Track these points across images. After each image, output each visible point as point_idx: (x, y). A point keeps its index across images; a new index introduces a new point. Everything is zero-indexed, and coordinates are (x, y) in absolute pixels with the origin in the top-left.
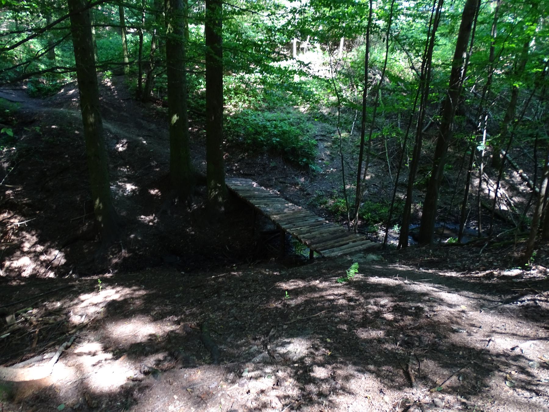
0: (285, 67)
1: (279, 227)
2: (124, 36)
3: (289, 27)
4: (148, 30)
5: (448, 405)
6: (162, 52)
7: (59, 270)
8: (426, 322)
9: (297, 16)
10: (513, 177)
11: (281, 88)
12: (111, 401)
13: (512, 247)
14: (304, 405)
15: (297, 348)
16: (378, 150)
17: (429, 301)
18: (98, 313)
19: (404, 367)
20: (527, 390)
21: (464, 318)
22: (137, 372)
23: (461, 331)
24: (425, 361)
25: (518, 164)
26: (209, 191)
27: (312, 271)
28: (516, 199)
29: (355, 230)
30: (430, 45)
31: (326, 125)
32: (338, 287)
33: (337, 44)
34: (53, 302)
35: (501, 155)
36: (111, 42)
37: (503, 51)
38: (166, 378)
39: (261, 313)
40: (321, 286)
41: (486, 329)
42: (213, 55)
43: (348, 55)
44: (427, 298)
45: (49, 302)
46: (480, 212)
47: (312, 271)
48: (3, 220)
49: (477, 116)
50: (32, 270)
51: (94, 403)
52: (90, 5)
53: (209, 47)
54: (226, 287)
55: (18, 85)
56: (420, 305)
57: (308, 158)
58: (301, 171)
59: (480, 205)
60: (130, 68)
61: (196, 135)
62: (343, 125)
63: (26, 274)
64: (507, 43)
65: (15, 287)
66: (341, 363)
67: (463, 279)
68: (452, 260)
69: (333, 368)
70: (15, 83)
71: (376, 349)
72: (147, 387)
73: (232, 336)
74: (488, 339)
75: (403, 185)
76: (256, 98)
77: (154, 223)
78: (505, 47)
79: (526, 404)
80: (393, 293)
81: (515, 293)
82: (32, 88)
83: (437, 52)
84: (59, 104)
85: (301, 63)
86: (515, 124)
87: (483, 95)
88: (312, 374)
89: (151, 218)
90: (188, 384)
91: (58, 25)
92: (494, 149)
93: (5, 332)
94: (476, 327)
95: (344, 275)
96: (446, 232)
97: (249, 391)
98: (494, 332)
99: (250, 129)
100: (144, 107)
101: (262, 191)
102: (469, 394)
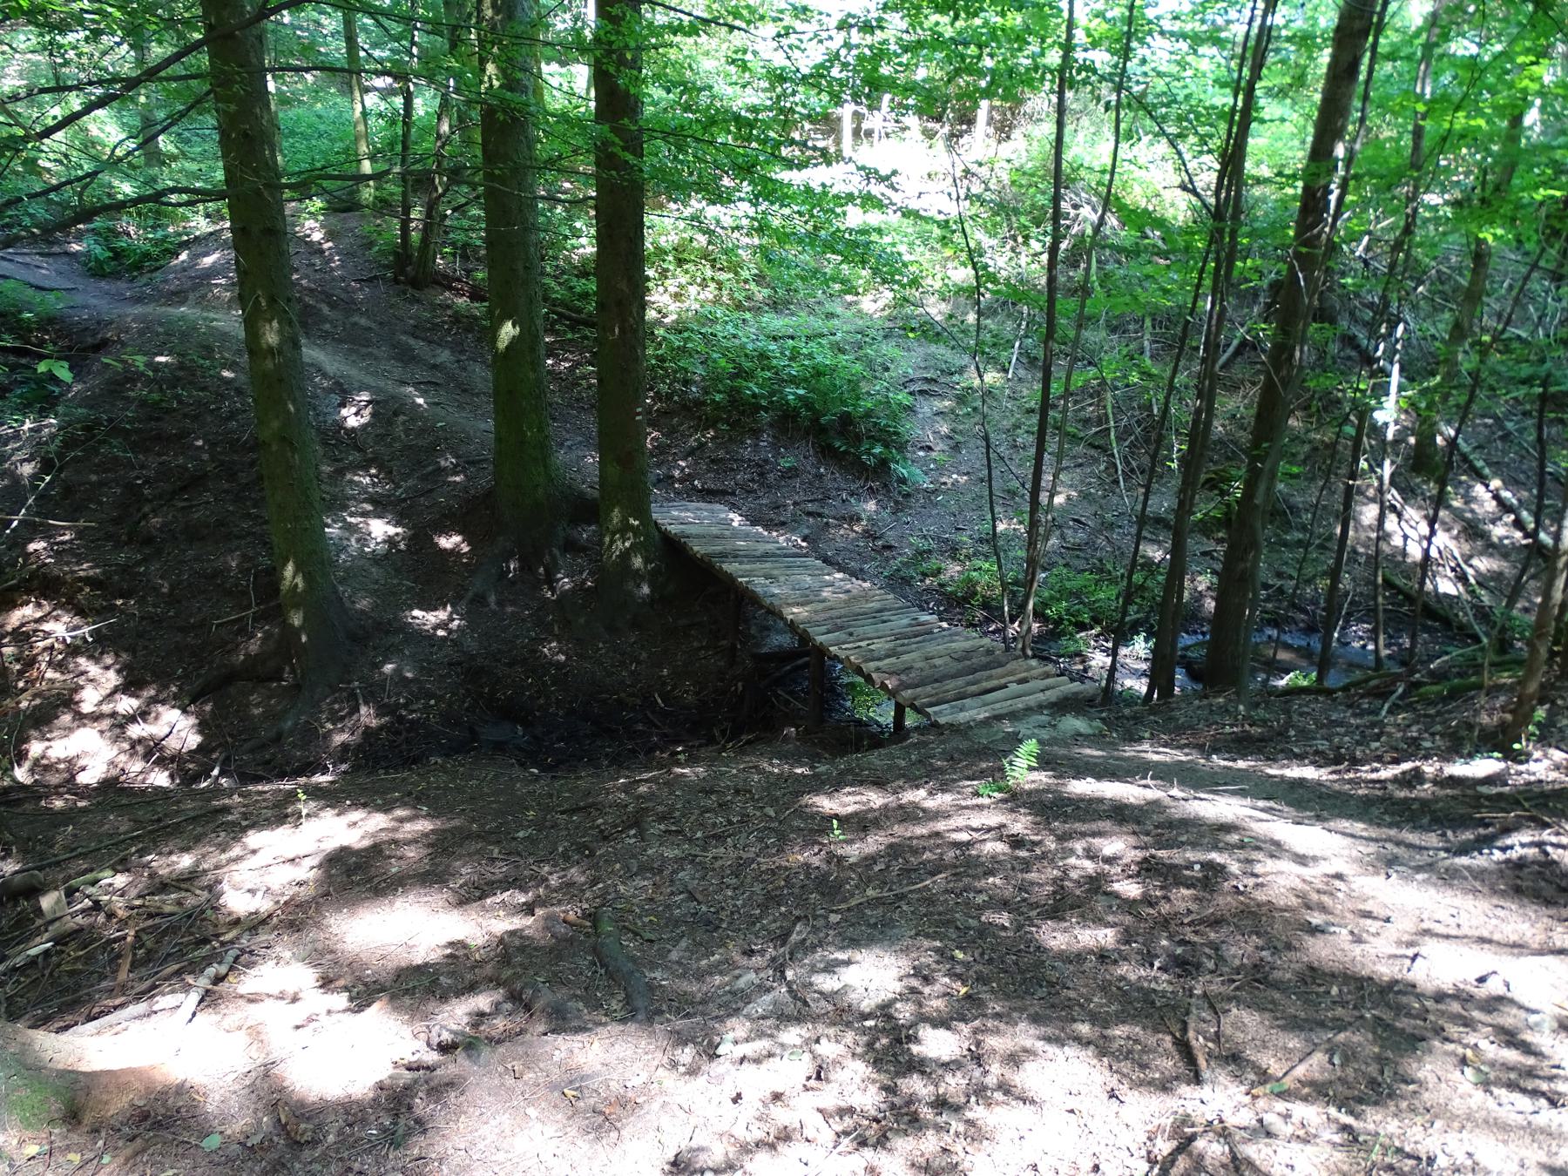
0: (824, 185)
1: (804, 638)
2: (353, 101)
3: (835, 72)
4: (431, 80)
5: (1301, 1133)
6: (467, 142)
7: (186, 767)
8: (1234, 904)
9: (856, 37)
10: (1475, 499)
11: (812, 244)
12: (350, 1125)
13: (1473, 698)
14: (897, 1132)
15: (873, 975)
16: (1086, 422)
17: (1242, 846)
18: (300, 884)
19: (1176, 1028)
20: (1524, 1091)
21: (1340, 895)
22: (420, 1044)
23: (1332, 929)
24: (1235, 1011)
25: (1489, 464)
26: (607, 539)
27: (903, 763)
28: (1483, 564)
29: (1023, 649)
30: (1242, 120)
31: (940, 350)
32: (980, 807)
33: (968, 120)
34: (171, 853)
35: (1439, 439)
36: (320, 117)
37: (1446, 140)
38: (502, 1062)
39: (763, 881)
40: (930, 804)
41: (1404, 925)
42: (617, 150)
43: (1004, 153)
44: (1234, 838)
45: (160, 854)
46: (1380, 599)
47: (903, 763)
48: (23, 625)
49: (1372, 327)
50: (105, 768)
51: (305, 1131)
52: (264, 13)
53: (606, 128)
54: (660, 809)
55: (57, 242)
56: (1215, 856)
57: (886, 446)
58: (867, 480)
59: (1380, 580)
60: (377, 189)
61: (569, 382)
62: (985, 352)
63: (88, 778)
64: (1461, 114)
65: (61, 812)
66: (998, 1016)
67: (1337, 786)
68: (1304, 734)
69: (975, 1031)
70: (50, 235)
71: (1095, 979)
72: (451, 1084)
73: (683, 944)
74: (1410, 952)
75: (1159, 521)
76: (736, 273)
77: (450, 632)
78: (1457, 127)
79: (1523, 1128)
80: (1138, 823)
81: (1487, 826)
82: (98, 250)
83: (1258, 142)
84: (174, 293)
85: (870, 174)
86: (1484, 350)
87: (1392, 266)
88: (915, 1049)
89: (442, 615)
90: (566, 1077)
91: (176, 69)
92: (1421, 420)
93: (38, 939)
94: (1375, 918)
95: (997, 774)
96: (1283, 656)
97: (739, 1096)
98: (1427, 932)
99: (723, 362)
100: (418, 301)
101: (758, 539)
102: (1360, 1101)
